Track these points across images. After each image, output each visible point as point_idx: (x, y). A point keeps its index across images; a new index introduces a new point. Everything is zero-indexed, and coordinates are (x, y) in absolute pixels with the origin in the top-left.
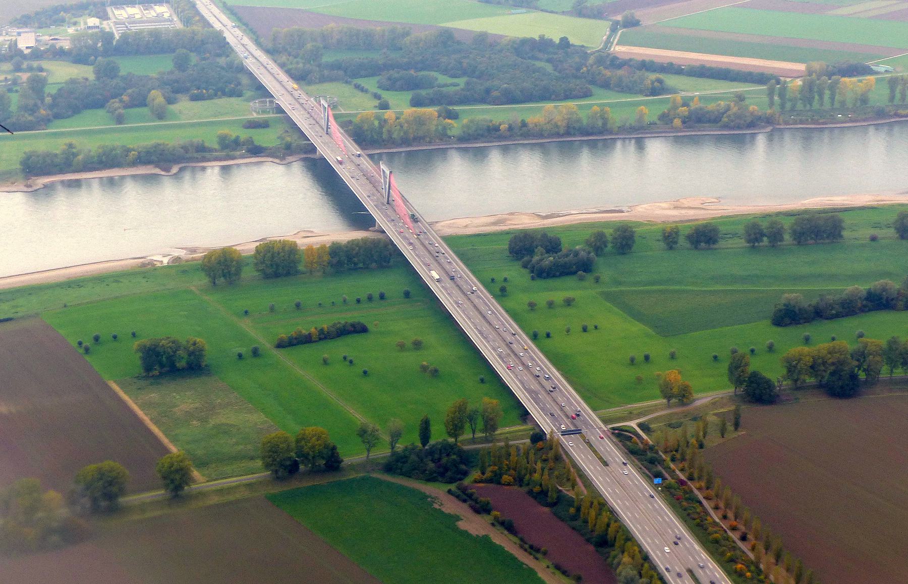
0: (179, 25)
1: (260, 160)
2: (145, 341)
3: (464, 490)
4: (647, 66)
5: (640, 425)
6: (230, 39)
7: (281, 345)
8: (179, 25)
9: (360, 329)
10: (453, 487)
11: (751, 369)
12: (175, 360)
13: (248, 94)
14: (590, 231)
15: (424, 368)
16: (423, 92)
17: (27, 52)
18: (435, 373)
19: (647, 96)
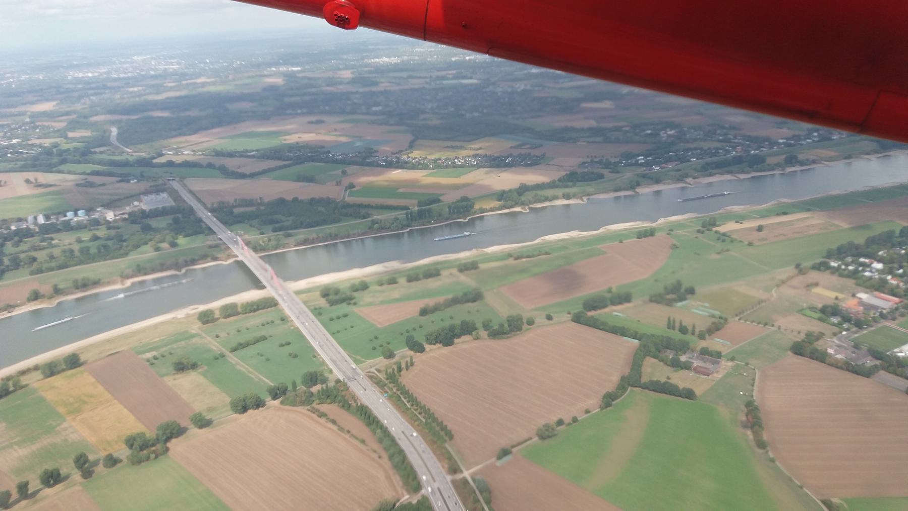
0: (173, 204)
1: (273, 129)
2: (124, 438)
3: (313, 408)
4: (360, 206)
5: (376, 370)
6: (195, 207)
7: (234, 350)
8: (173, 204)
9: (264, 338)
10: (308, 407)
11: (415, 339)
12: (607, 160)
13: (206, 232)
14: (359, 280)
15: (290, 355)
16: (277, 225)
17: (111, 220)
18: (296, 356)
19: (362, 219)
